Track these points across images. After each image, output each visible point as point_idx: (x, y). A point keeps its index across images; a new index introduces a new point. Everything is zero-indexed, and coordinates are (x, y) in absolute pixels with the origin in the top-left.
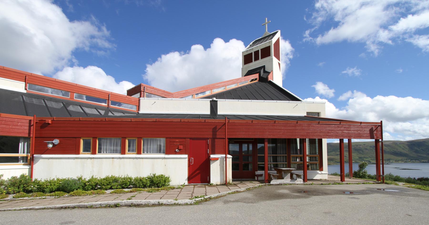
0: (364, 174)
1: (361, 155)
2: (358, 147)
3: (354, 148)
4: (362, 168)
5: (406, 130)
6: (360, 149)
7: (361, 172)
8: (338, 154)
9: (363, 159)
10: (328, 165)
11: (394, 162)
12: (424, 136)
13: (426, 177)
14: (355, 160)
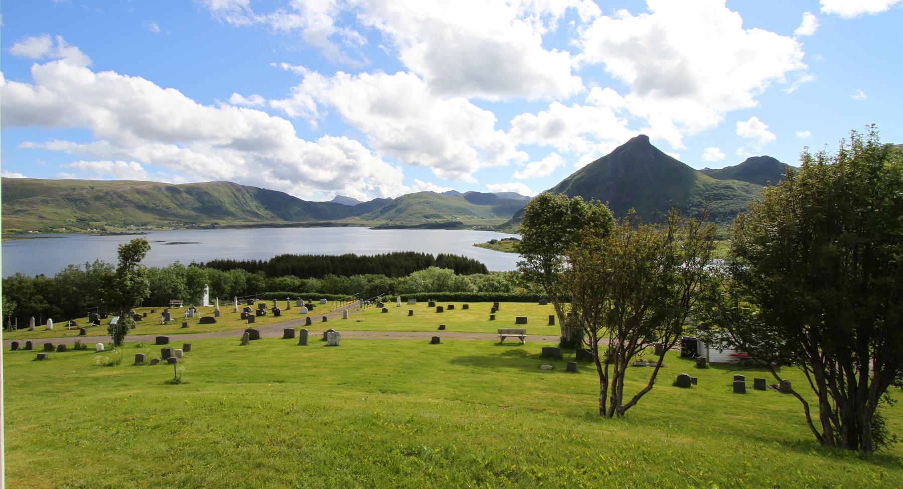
0: (138, 283)
1: (84, 213)
2: (76, 193)
3: (65, 196)
4: (133, 260)
5: (171, 162)
6: (81, 198)
7: (129, 276)
8: (19, 211)
9: (88, 224)
10: (2, 214)
11: (154, 229)
12: (204, 177)
13: (221, 260)
14: (68, 225)
